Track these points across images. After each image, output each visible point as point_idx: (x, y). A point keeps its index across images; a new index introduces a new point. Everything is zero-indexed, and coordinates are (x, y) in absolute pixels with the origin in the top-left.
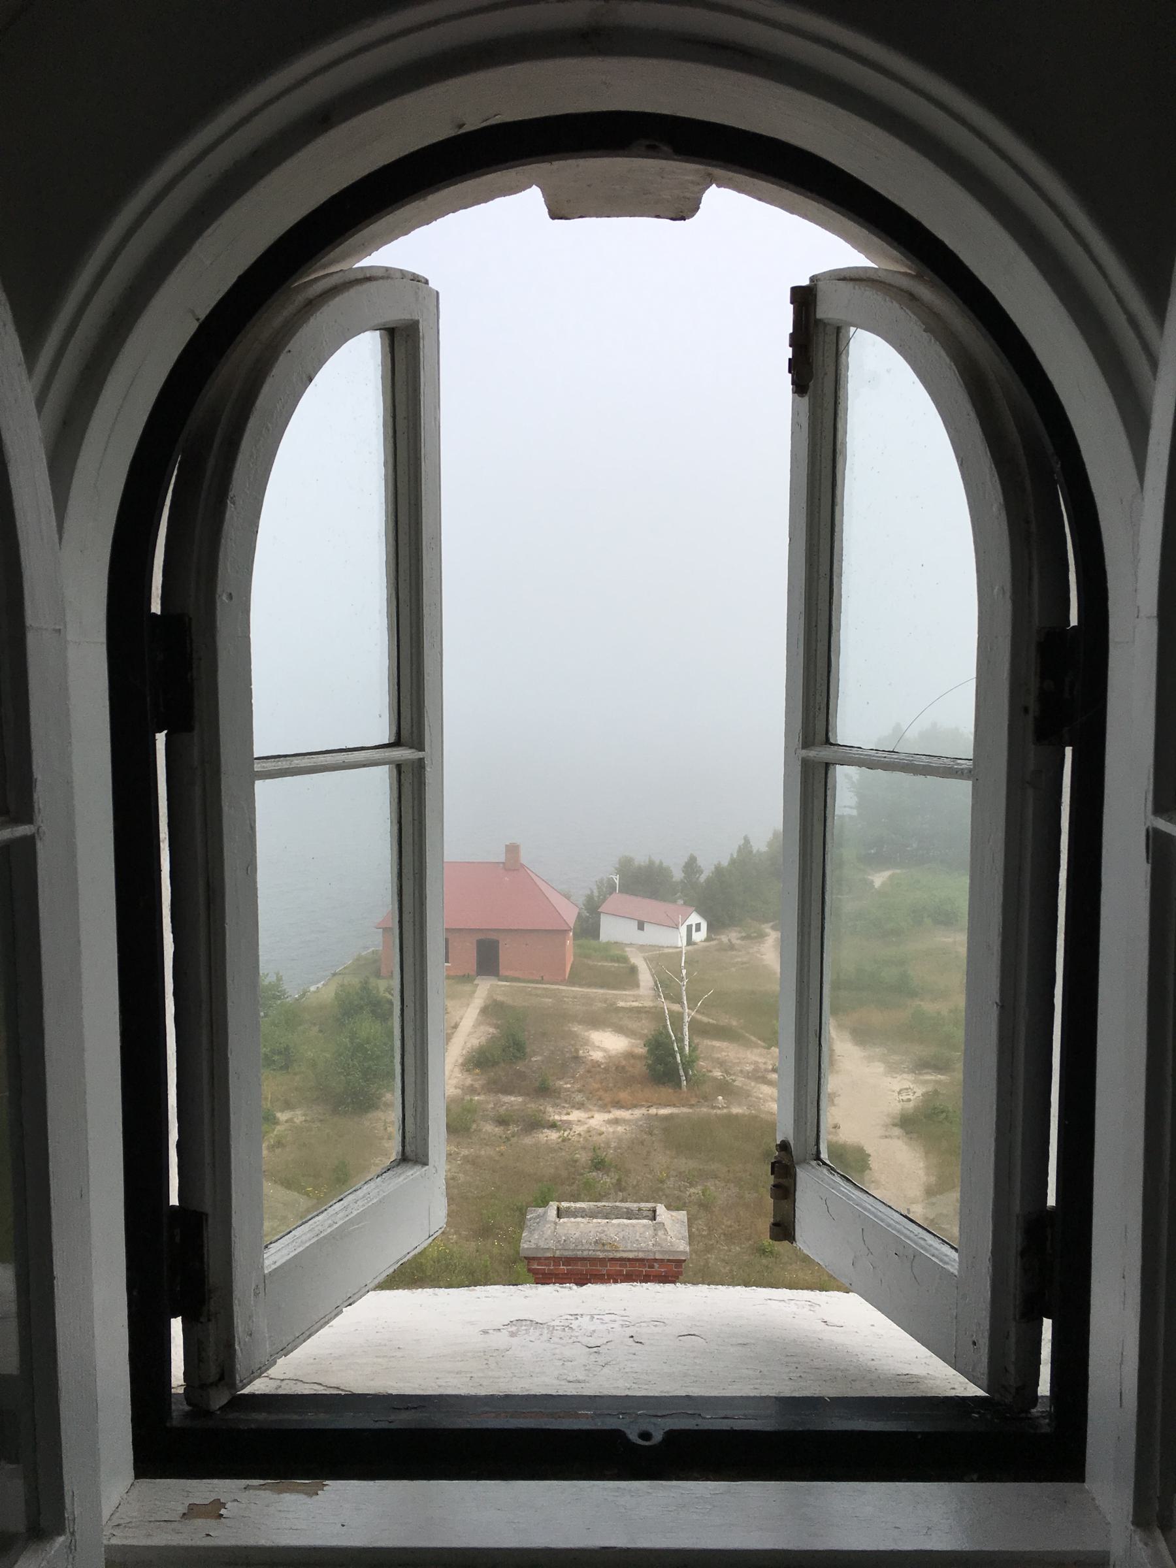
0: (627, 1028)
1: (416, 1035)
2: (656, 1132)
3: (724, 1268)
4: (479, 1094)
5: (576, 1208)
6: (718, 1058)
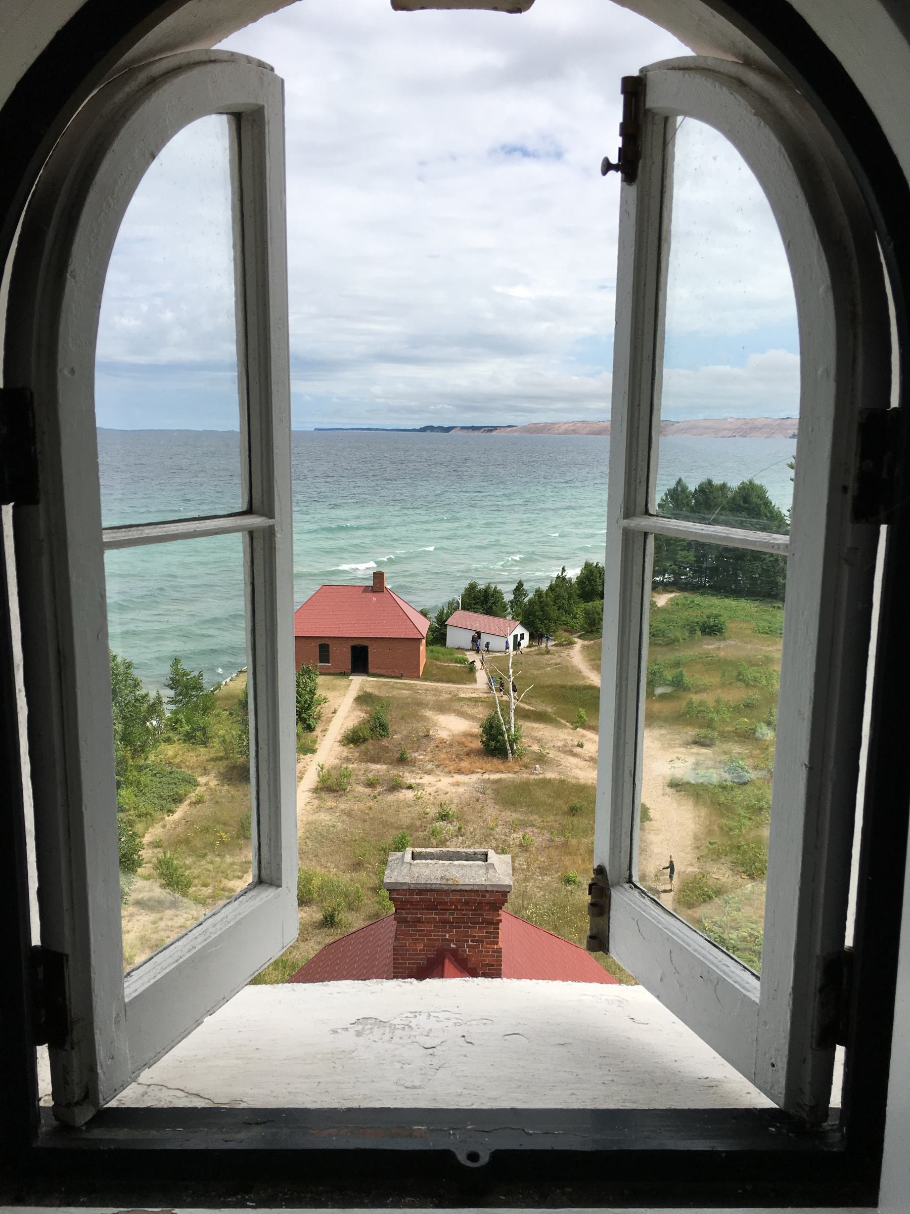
0: (467, 714)
1: (269, 773)
2: (488, 791)
3: (539, 892)
4: (353, 763)
5: (426, 853)
6: (537, 737)
